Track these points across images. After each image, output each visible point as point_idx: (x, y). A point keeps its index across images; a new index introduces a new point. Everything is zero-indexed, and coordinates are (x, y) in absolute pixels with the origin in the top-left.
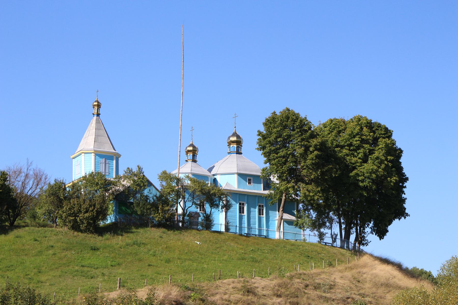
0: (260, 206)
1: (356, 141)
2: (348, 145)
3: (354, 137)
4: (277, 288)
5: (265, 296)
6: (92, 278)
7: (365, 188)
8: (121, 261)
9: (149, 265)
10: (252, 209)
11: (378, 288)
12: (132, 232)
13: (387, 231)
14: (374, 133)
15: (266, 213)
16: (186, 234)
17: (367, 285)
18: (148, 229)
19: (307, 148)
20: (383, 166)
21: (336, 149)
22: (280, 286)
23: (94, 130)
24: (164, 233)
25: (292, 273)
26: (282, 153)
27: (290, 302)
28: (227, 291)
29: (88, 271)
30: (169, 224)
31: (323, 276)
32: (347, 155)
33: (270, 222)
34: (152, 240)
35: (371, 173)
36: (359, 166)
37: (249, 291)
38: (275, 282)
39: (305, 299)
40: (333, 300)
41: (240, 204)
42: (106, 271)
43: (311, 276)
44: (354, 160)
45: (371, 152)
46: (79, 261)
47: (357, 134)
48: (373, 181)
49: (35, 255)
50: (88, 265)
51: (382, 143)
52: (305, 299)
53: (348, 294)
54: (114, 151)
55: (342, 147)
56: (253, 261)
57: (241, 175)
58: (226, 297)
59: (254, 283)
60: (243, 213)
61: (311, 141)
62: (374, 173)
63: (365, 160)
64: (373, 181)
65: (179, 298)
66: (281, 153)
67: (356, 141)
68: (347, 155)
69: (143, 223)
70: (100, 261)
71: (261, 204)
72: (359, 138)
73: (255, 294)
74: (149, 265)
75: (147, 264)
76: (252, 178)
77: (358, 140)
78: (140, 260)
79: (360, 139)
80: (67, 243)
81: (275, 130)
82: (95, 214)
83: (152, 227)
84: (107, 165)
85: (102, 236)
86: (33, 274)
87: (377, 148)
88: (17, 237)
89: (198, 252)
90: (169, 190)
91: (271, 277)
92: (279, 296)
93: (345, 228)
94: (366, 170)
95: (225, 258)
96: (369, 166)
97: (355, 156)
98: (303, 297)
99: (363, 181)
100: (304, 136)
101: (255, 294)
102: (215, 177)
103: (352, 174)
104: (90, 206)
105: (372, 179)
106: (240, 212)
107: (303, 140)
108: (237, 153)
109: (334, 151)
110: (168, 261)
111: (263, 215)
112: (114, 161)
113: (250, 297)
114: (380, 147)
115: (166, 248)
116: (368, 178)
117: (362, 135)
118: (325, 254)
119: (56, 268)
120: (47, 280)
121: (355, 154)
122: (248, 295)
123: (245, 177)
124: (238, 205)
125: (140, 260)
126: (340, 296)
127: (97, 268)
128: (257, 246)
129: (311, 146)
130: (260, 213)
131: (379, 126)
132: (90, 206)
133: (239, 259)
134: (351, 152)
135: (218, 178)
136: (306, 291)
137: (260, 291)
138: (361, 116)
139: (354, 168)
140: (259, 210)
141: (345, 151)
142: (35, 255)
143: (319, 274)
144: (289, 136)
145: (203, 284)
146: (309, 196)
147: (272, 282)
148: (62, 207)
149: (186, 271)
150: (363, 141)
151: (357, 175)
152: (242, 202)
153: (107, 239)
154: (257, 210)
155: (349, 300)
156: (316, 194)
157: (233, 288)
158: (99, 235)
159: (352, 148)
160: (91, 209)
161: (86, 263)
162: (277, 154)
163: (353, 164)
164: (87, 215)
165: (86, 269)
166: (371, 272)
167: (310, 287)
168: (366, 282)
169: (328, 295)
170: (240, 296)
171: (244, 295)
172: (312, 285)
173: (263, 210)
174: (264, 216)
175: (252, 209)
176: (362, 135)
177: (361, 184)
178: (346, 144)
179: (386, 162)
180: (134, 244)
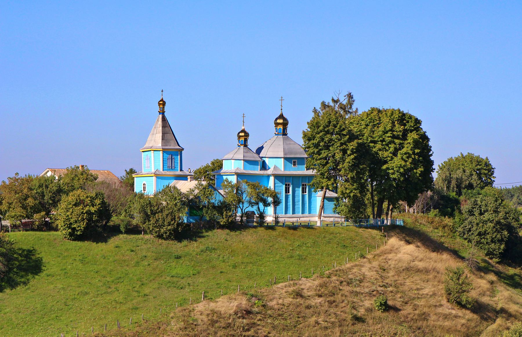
0: (303, 185)
1: (388, 137)
2: (381, 141)
3: (387, 132)
4: (318, 288)
5: (309, 296)
6: (181, 288)
7: (395, 179)
8: (199, 268)
9: (221, 272)
10: (296, 189)
11: (399, 276)
12: (204, 237)
13: (431, 147)
14: (405, 125)
15: (309, 191)
16: (245, 233)
17: (391, 273)
18: (215, 230)
19: (344, 151)
20: (410, 160)
21: (371, 144)
22: (321, 286)
23: (161, 128)
24: (228, 234)
25: (330, 271)
26: (324, 154)
27: (328, 301)
28: (281, 296)
29: (177, 281)
30: (233, 226)
31: (355, 270)
32: (380, 150)
33: (312, 198)
34: (219, 244)
35: (399, 167)
36: (390, 160)
37: (299, 294)
38: (317, 282)
39: (339, 296)
40: (362, 294)
41: (286, 185)
42: (190, 280)
43: (345, 272)
44: (386, 154)
45: (402, 146)
46: (168, 271)
47: (390, 130)
48: (402, 174)
49: (134, 266)
50: (176, 275)
51: (412, 136)
52: (339, 296)
53: (374, 288)
54: (178, 147)
55: (375, 142)
56: (299, 259)
57: (286, 159)
58: (280, 301)
59: (301, 285)
60: (289, 193)
61: (349, 144)
62: (402, 167)
63: (395, 154)
64: (402, 174)
65: (248, 307)
66: (323, 155)
67: (388, 137)
68: (380, 150)
69: (212, 225)
70: (184, 270)
71: (304, 183)
72: (391, 134)
73: (302, 296)
74: (221, 272)
75: (219, 272)
76: (296, 160)
77: (390, 137)
78: (214, 267)
79: (391, 135)
80: (156, 253)
81: (318, 135)
82: (175, 226)
83: (217, 229)
84: (173, 160)
85: (181, 242)
86: (138, 286)
87: (406, 142)
88: (117, 247)
89: (256, 254)
90: (232, 199)
91: (314, 276)
92: (320, 296)
93: (378, 201)
94: (395, 165)
95: (278, 257)
96: (397, 161)
97: (386, 151)
98: (338, 294)
99: (393, 174)
100: (342, 141)
101: (302, 296)
102: (264, 159)
103: (384, 167)
104: (172, 220)
105: (400, 173)
106: (286, 192)
107: (342, 144)
108: (283, 135)
109: (369, 146)
110: (235, 267)
111: (306, 192)
112: (179, 156)
113: (298, 300)
114: (408, 142)
115: (232, 251)
116: (398, 172)
117: (394, 131)
118: (358, 240)
119: (154, 280)
120: (150, 292)
121: (387, 148)
122: (297, 298)
123: (290, 160)
124: (284, 186)
125: (214, 267)
126: (367, 290)
127: (183, 278)
128: (302, 240)
129: (348, 149)
130: (304, 191)
131: (411, 117)
132: (172, 220)
133: (288, 258)
134: (383, 147)
135: (267, 160)
136: (341, 288)
137: (306, 293)
138: (393, 109)
139: (386, 162)
140: (303, 188)
141: (379, 146)
142: (134, 266)
143: (350, 269)
144: (331, 140)
145: (263, 290)
146: (346, 193)
147: (314, 282)
148: (149, 221)
149: (250, 277)
150: (394, 137)
151: (388, 168)
152: (287, 183)
153: (186, 246)
154: (301, 189)
155: (374, 293)
156: (351, 192)
157: (286, 292)
158: (178, 242)
159: (384, 143)
160: (172, 223)
161: (174, 273)
162: (319, 155)
163: (385, 158)
164: (169, 228)
165: (175, 279)
166: (396, 258)
167: (344, 283)
168: (390, 269)
169: (358, 289)
170: (291, 300)
171: (293, 298)
172: (345, 281)
173: (306, 188)
174: (307, 193)
175: (296, 189)
176: (394, 131)
177: (391, 176)
178: (379, 140)
179: (413, 156)
180: (206, 250)
